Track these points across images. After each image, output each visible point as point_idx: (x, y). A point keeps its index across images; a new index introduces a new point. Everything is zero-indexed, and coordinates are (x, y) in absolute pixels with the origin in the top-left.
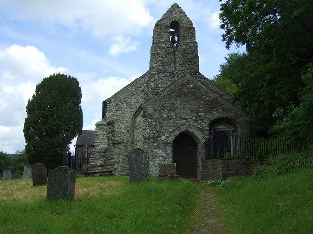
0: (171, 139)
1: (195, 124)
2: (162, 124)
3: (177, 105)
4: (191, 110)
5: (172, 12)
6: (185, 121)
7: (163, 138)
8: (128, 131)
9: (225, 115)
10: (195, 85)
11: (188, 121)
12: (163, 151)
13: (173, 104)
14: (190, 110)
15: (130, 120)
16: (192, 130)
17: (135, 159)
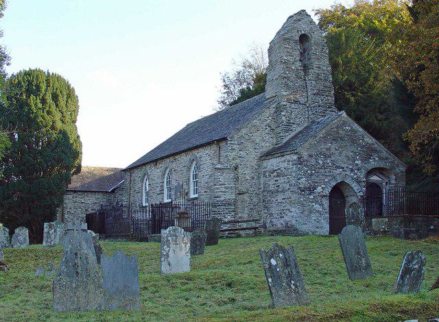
0: (327, 191)
1: (352, 174)
3: (333, 150)
6: (341, 170)
7: (319, 189)
9: (382, 165)
12: (320, 205)
15: (254, 163)
17: (353, 214)
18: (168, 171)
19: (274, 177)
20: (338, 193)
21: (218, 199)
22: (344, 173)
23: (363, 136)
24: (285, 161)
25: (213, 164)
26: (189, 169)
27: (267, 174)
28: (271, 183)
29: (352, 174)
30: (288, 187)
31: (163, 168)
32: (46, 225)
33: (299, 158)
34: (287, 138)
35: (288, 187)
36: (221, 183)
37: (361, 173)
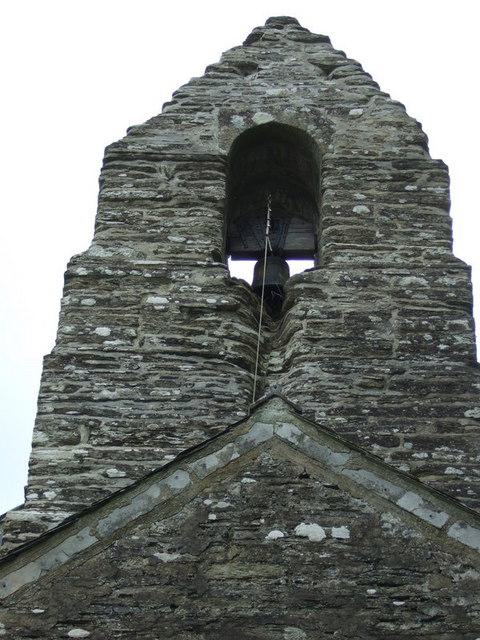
5: (247, 68)
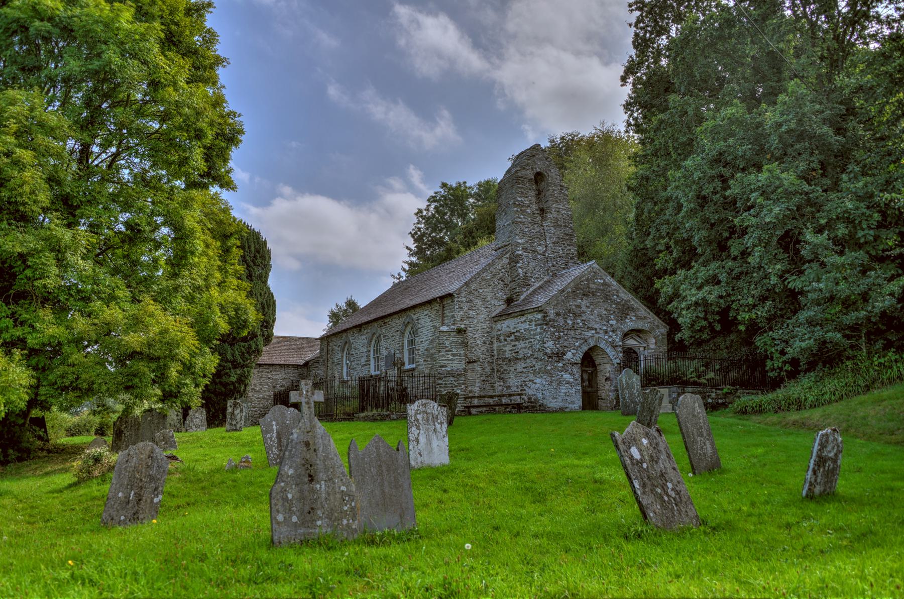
1: (606, 337)
2: (567, 335)
3: (584, 308)
4: (601, 316)
6: (593, 332)
7: (569, 355)
8: (484, 343)
9: (640, 325)
10: (604, 281)
11: (598, 333)
12: (571, 374)
13: (579, 306)
14: (600, 315)
16: (602, 345)
18: (375, 338)
19: (512, 341)
20: (589, 361)
21: (444, 369)
22: (597, 336)
23: (618, 292)
24: (525, 321)
25: (434, 327)
26: (403, 334)
27: (502, 338)
28: (507, 349)
29: (606, 337)
30: (530, 352)
31: (370, 334)
32: (230, 403)
33: (544, 317)
34: (525, 295)
35: (530, 352)
36: (447, 349)
37: (617, 335)
